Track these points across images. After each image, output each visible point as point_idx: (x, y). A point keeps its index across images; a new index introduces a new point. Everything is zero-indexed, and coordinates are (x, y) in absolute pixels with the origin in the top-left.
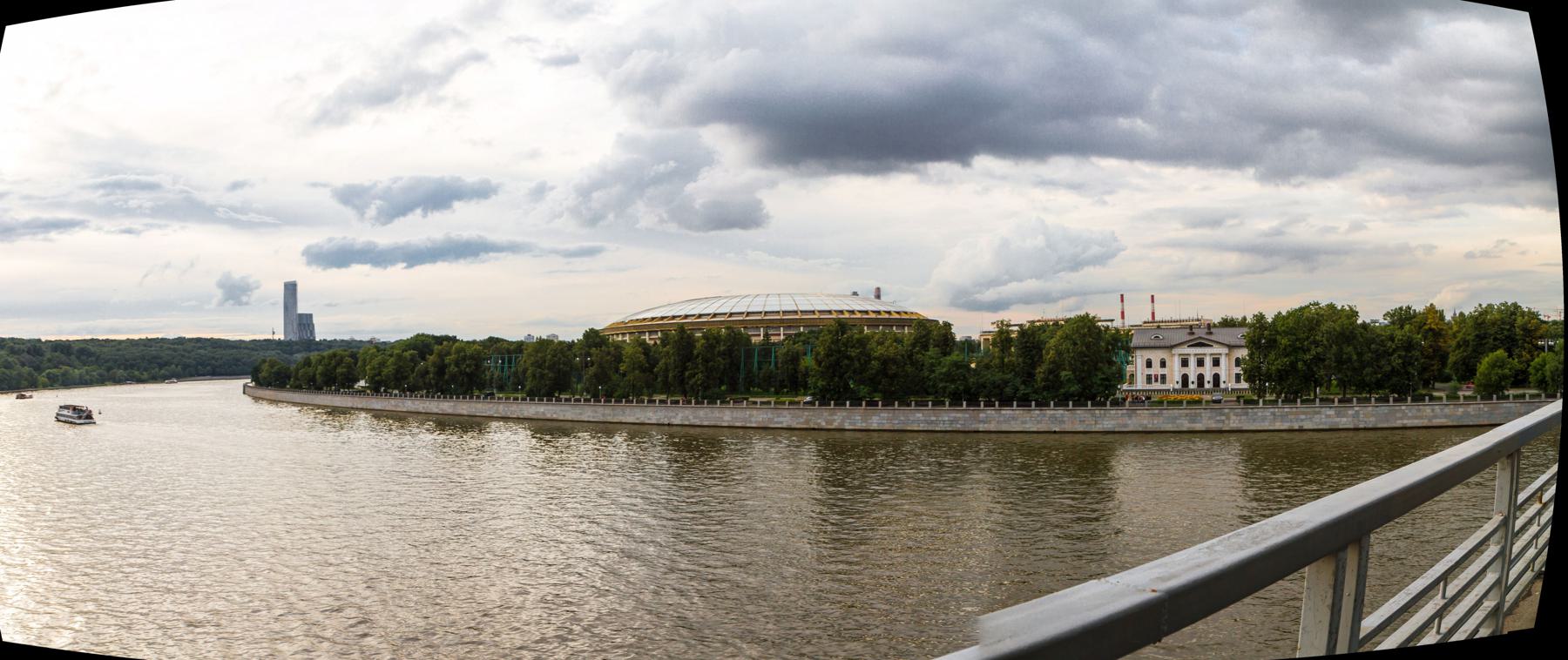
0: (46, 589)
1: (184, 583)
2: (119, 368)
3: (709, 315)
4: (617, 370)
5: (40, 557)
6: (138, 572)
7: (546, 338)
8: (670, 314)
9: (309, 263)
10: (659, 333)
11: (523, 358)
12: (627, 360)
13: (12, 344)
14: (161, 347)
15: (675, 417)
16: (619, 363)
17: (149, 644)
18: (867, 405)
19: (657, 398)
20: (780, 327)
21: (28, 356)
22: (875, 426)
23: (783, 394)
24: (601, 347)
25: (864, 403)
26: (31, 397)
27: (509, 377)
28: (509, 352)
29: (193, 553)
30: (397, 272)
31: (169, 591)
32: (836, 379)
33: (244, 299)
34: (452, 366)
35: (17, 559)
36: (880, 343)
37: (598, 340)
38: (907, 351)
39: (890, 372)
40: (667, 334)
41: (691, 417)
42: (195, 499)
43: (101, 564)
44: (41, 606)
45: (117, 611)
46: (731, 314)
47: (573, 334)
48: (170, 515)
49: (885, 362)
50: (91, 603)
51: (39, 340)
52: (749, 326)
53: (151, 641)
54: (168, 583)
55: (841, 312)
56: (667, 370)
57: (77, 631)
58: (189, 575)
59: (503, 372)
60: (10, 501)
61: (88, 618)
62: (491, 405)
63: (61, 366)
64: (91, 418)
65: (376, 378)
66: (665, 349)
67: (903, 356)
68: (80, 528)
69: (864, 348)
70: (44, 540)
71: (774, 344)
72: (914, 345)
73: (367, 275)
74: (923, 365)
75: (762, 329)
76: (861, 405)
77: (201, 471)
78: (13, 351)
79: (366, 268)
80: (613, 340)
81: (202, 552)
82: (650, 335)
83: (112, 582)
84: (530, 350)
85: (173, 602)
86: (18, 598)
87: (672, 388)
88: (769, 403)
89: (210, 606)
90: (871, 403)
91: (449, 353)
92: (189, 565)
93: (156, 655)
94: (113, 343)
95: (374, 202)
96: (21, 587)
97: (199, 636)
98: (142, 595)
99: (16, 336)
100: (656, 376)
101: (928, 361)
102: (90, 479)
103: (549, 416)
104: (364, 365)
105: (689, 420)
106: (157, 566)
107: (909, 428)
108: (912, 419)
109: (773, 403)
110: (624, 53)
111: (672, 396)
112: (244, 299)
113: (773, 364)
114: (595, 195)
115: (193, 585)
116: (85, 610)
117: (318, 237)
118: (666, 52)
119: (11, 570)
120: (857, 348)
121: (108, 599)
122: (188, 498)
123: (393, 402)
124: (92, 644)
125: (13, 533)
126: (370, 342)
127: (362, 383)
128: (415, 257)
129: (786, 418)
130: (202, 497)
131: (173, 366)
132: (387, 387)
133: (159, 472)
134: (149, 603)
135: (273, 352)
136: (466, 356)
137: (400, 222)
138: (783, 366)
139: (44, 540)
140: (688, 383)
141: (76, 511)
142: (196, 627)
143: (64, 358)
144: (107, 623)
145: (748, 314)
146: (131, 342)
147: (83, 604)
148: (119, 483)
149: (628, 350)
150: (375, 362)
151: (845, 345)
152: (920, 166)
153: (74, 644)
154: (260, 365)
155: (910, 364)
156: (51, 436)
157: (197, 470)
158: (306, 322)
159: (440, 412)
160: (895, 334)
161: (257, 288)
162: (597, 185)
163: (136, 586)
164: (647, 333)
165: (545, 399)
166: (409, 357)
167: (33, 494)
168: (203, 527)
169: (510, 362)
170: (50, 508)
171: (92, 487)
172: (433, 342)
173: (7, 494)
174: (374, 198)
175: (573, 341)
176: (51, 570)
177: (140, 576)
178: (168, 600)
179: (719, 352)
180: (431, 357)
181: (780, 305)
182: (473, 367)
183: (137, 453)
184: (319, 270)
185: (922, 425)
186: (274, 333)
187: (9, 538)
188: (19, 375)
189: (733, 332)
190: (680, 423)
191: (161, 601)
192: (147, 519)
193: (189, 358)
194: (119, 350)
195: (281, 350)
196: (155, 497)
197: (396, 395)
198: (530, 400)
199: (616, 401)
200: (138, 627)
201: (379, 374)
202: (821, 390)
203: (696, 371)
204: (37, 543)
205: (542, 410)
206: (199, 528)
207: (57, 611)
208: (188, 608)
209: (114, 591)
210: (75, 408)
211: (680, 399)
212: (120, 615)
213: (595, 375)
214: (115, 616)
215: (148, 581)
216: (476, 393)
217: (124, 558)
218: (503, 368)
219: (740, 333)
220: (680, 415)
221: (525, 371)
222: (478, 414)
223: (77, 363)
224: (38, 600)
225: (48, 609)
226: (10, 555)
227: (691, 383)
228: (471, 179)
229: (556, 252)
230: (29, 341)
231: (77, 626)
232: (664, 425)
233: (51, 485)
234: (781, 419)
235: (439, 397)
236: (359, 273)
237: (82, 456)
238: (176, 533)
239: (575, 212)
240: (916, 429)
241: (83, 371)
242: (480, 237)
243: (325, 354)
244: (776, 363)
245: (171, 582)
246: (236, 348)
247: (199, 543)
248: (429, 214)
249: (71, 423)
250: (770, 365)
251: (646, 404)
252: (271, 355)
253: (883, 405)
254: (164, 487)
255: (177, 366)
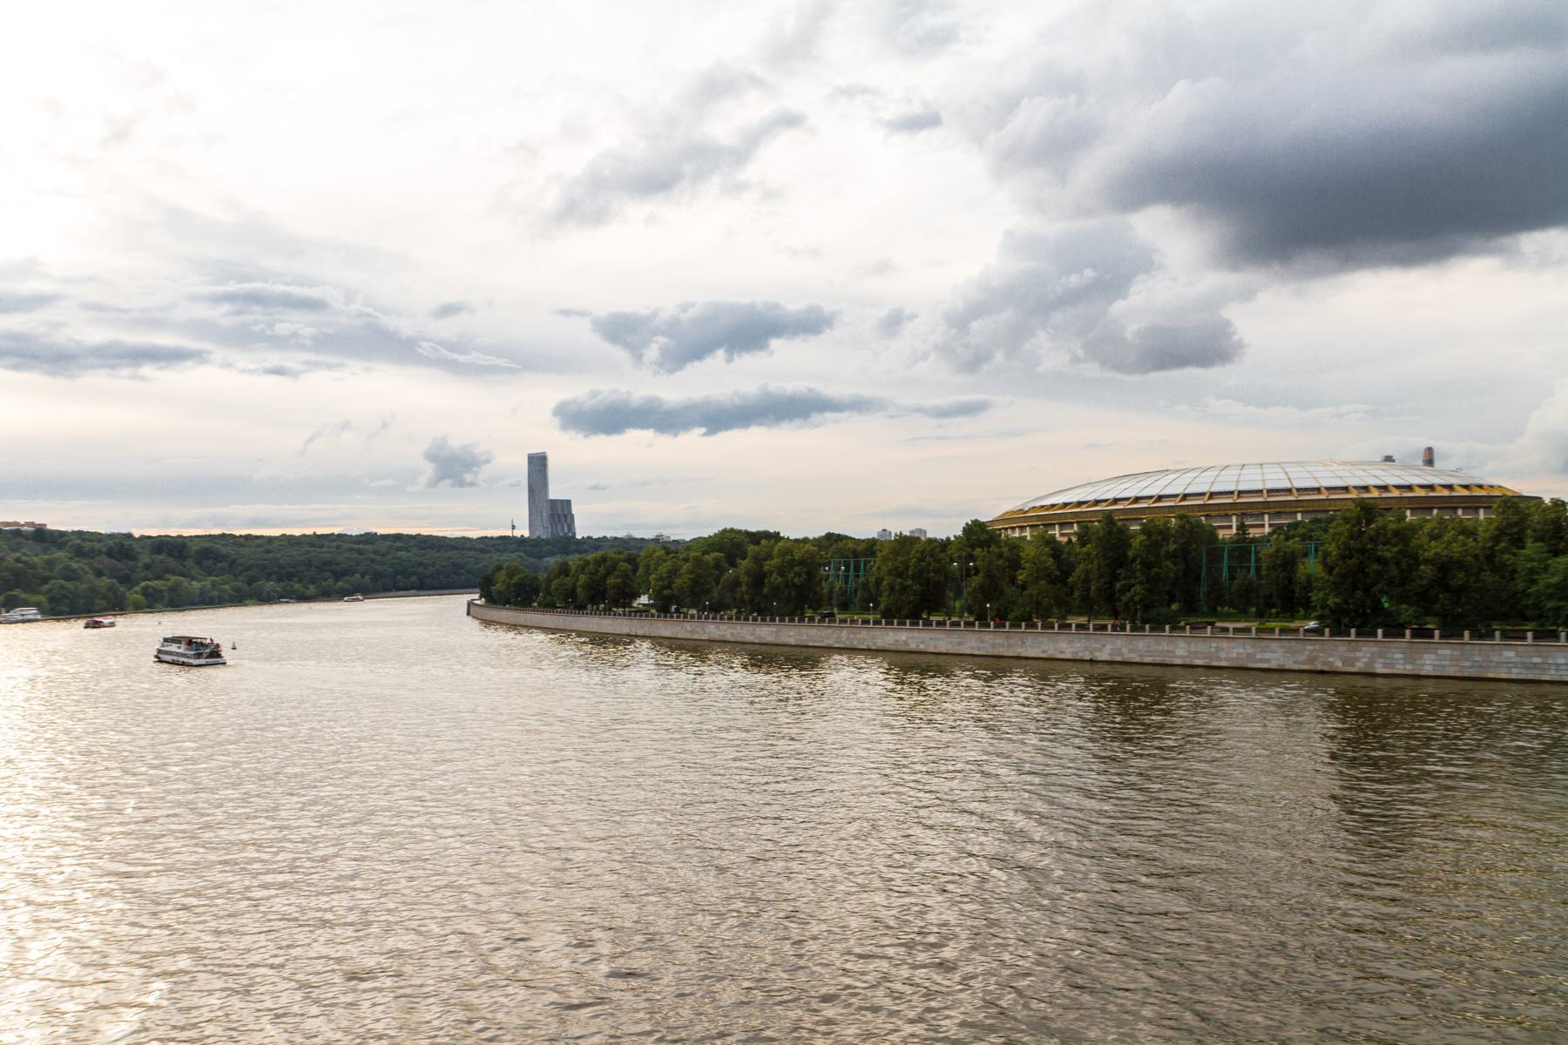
0: (106, 939)
1: (350, 909)
2: (268, 578)
3: (1151, 497)
4: (1013, 581)
5: (103, 886)
6: (276, 896)
7: (908, 534)
8: (1091, 498)
9: (565, 427)
10: (1075, 526)
11: (876, 563)
12: (1027, 565)
13: (79, 541)
14: (338, 547)
15: (1099, 650)
16: (1016, 570)
17: (277, 1016)
18: (1414, 635)
19: (1074, 621)
20: (1263, 514)
21: (107, 561)
22: (1428, 670)
23: (1270, 616)
24: (989, 547)
25: (1408, 632)
26: (112, 625)
27: (856, 590)
28: (855, 554)
29: (372, 859)
30: (693, 440)
31: (324, 923)
32: (1359, 594)
33: (468, 477)
34: (775, 575)
35: (58, 893)
36: (1434, 537)
37: (984, 537)
38: (1483, 548)
39: (1453, 583)
40: (1087, 527)
41: (1125, 650)
42: (383, 776)
43: (215, 887)
44: (91, 970)
45: (229, 966)
46: (1185, 497)
47: (948, 529)
48: (342, 802)
49: (1445, 567)
50: (186, 956)
51: (129, 536)
52: (1213, 513)
53: (281, 1011)
54: (326, 910)
55: (1366, 488)
56: (1087, 581)
57: (151, 1008)
58: (362, 896)
59: (846, 583)
60: (58, 795)
61: (175, 983)
62: (830, 631)
63: (167, 576)
64: (219, 656)
65: (665, 592)
66: (1084, 549)
67: (1476, 557)
68: (184, 831)
69: (1407, 545)
70: (114, 856)
71: (1254, 540)
72: (1496, 539)
73: (651, 445)
74: (1514, 571)
75: (1234, 518)
76: (1403, 636)
77: (396, 732)
78: (79, 552)
79: (648, 435)
80: (1007, 536)
81: (386, 857)
82: (1061, 529)
83: (229, 916)
84: (885, 552)
85: (329, 942)
86: (48, 961)
87: (1095, 607)
88: (1247, 630)
89: (391, 943)
90: (1422, 633)
91: (769, 557)
92: (363, 879)
93: (286, 1035)
94: (259, 542)
95: (655, 339)
96: (57, 942)
97: (364, 996)
98: (278, 935)
99: (85, 529)
100: (1072, 588)
101: (1523, 566)
102: (209, 751)
103: (913, 646)
104: (647, 573)
105: (1122, 655)
106: (309, 885)
107: (1491, 675)
108: (1495, 659)
109: (1254, 629)
110: (1010, 104)
111: (1096, 619)
112: (468, 477)
113: (1253, 571)
114: (975, 325)
115: (365, 912)
116: (173, 969)
117: (577, 390)
118: (1073, 98)
119: (44, 913)
120: (1394, 545)
121: (218, 945)
122: (372, 774)
123: (688, 626)
124: (174, 1027)
125: (57, 849)
126: (656, 540)
127: (644, 599)
128: (718, 418)
129: (1275, 654)
130: (395, 772)
131: (358, 575)
132: (680, 605)
133: (327, 737)
134: (288, 946)
135: (514, 556)
136: (793, 560)
137: (694, 369)
138: (1268, 575)
139: (114, 856)
140: (1119, 600)
141: (180, 804)
142: (362, 980)
143: (172, 563)
144: (209, 987)
145: (1212, 495)
146: (369, 538)
147: (170, 959)
148: (260, 755)
149: (1029, 552)
150: (664, 569)
151: (1373, 540)
152: (1506, 241)
153: (138, 1032)
154: (494, 573)
155: (1491, 570)
156: (147, 686)
157: (391, 731)
158: (561, 512)
159: (756, 641)
160: (1462, 521)
161: (488, 461)
162: (978, 310)
163: (269, 920)
164: (1057, 526)
165: (908, 621)
166: (712, 562)
167: (104, 780)
168: (392, 817)
169: (857, 569)
170: (132, 802)
171: (212, 764)
172: (747, 540)
173: (54, 784)
174: (655, 333)
175: (948, 539)
176: (120, 905)
177: (279, 904)
178: (322, 939)
179: (1168, 552)
180: (744, 562)
181: (1264, 481)
182: (805, 577)
183: (294, 708)
184: (580, 436)
185: (1514, 670)
186: (513, 527)
187: (48, 857)
188: (93, 590)
189: (1188, 521)
190: (1107, 658)
191: (308, 941)
192: (302, 810)
193: (383, 563)
194: (268, 552)
195: (524, 552)
196: (318, 776)
197: (693, 617)
198: (887, 624)
199: (1012, 626)
200: (262, 989)
201: (669, 587)
202: (1333, 612)
203: (1132, 581)
204: (101, 863)
205: (904, 638)
206: (386, 821)
207: (119, 977)
208: (353, 949)
209: (231, 932)
210: (190, 642)
211: (1109, 623)
212: (235, 971)
213: (982, 588)
214: (225, 974)
215: (292, 909)
216: (809, 613)
217: (255, 875)
218: (847, 577)
219: (1199, 525)
220: (1108, 647)
221: (879, 582)
222: (811, 644)
223: (196, 571)
224: (86, 961)
225: (102, 975)
226: (47, 886)
227: (1124, 599)
228: (793, 305)
229: (919, 410)
230: (112, 536)
231: (151, 1000)
232: (1082, 661)
233: (139, 764)
234: (1268, 656)
235: (755, 619)
236: (637, 444)
237: (198, 717)
238: (348, 830)
239: (946, 350)
240: (1504, 676)
241: (208, 582)
242: (810, 390)
243: (590, 557)
244: (1258, 569)
245: (330, 910)
246: (455, 548)
247: (384, 844)
248: (735, 357)
249: (183, 664)
250: (1249, 572)
251: (1056, 630)
252: (510, 558)
253: (1442, 637)
254: (335, 758)
255: (363, 576)
